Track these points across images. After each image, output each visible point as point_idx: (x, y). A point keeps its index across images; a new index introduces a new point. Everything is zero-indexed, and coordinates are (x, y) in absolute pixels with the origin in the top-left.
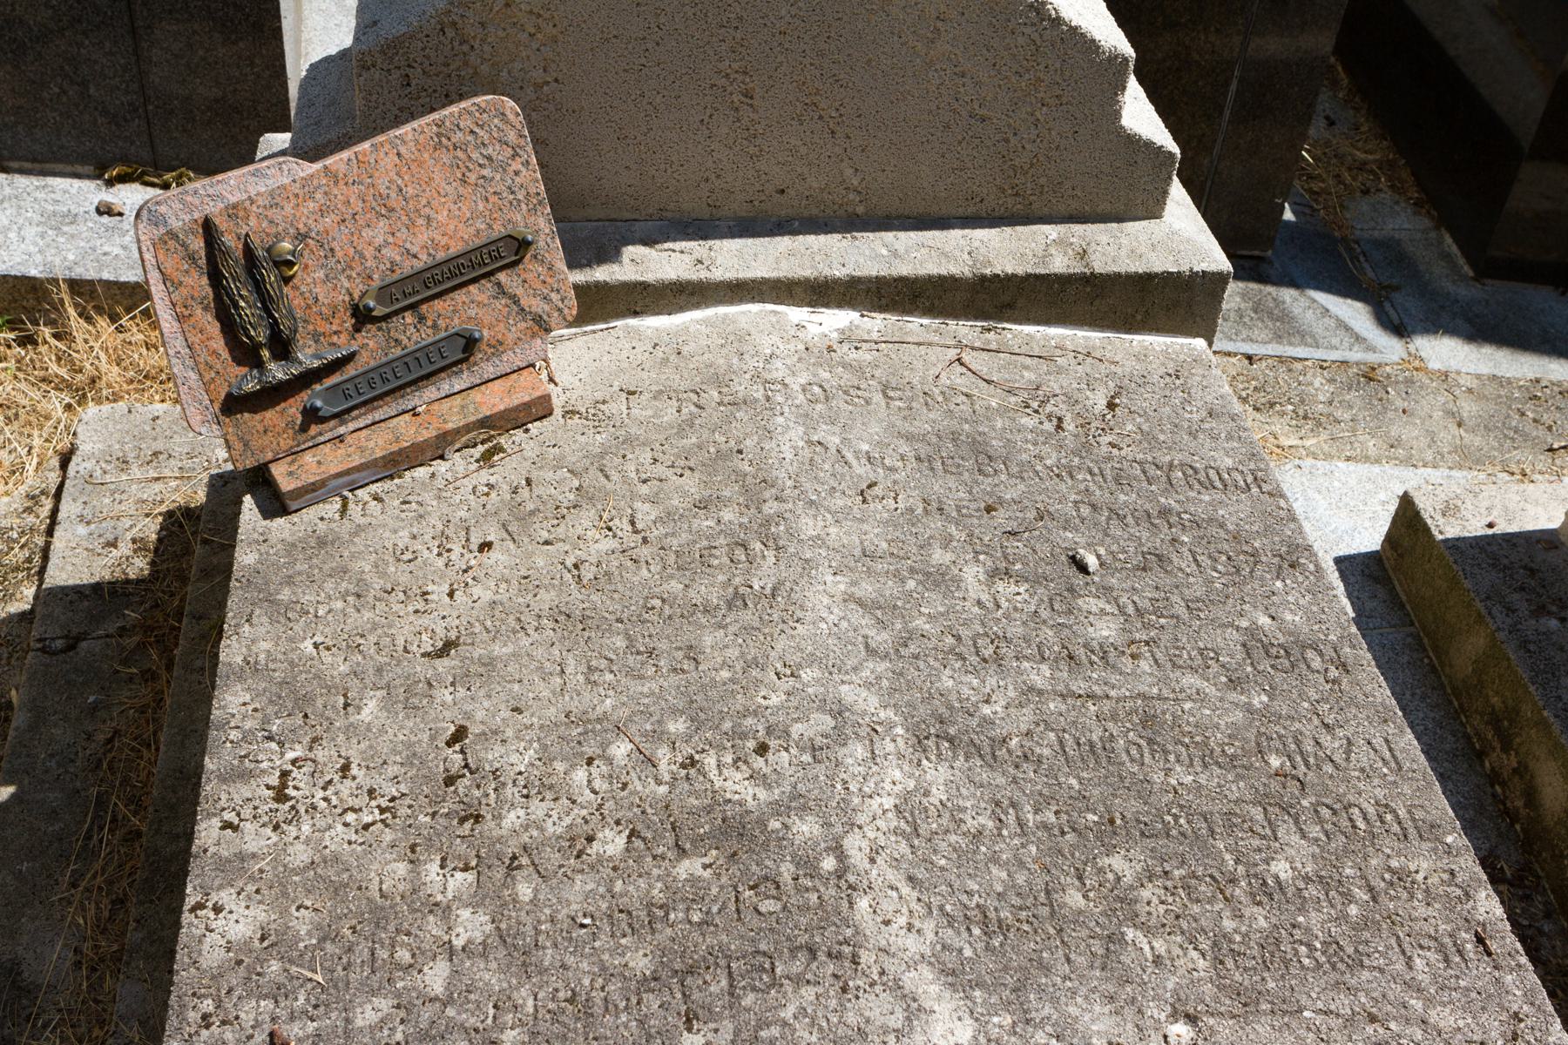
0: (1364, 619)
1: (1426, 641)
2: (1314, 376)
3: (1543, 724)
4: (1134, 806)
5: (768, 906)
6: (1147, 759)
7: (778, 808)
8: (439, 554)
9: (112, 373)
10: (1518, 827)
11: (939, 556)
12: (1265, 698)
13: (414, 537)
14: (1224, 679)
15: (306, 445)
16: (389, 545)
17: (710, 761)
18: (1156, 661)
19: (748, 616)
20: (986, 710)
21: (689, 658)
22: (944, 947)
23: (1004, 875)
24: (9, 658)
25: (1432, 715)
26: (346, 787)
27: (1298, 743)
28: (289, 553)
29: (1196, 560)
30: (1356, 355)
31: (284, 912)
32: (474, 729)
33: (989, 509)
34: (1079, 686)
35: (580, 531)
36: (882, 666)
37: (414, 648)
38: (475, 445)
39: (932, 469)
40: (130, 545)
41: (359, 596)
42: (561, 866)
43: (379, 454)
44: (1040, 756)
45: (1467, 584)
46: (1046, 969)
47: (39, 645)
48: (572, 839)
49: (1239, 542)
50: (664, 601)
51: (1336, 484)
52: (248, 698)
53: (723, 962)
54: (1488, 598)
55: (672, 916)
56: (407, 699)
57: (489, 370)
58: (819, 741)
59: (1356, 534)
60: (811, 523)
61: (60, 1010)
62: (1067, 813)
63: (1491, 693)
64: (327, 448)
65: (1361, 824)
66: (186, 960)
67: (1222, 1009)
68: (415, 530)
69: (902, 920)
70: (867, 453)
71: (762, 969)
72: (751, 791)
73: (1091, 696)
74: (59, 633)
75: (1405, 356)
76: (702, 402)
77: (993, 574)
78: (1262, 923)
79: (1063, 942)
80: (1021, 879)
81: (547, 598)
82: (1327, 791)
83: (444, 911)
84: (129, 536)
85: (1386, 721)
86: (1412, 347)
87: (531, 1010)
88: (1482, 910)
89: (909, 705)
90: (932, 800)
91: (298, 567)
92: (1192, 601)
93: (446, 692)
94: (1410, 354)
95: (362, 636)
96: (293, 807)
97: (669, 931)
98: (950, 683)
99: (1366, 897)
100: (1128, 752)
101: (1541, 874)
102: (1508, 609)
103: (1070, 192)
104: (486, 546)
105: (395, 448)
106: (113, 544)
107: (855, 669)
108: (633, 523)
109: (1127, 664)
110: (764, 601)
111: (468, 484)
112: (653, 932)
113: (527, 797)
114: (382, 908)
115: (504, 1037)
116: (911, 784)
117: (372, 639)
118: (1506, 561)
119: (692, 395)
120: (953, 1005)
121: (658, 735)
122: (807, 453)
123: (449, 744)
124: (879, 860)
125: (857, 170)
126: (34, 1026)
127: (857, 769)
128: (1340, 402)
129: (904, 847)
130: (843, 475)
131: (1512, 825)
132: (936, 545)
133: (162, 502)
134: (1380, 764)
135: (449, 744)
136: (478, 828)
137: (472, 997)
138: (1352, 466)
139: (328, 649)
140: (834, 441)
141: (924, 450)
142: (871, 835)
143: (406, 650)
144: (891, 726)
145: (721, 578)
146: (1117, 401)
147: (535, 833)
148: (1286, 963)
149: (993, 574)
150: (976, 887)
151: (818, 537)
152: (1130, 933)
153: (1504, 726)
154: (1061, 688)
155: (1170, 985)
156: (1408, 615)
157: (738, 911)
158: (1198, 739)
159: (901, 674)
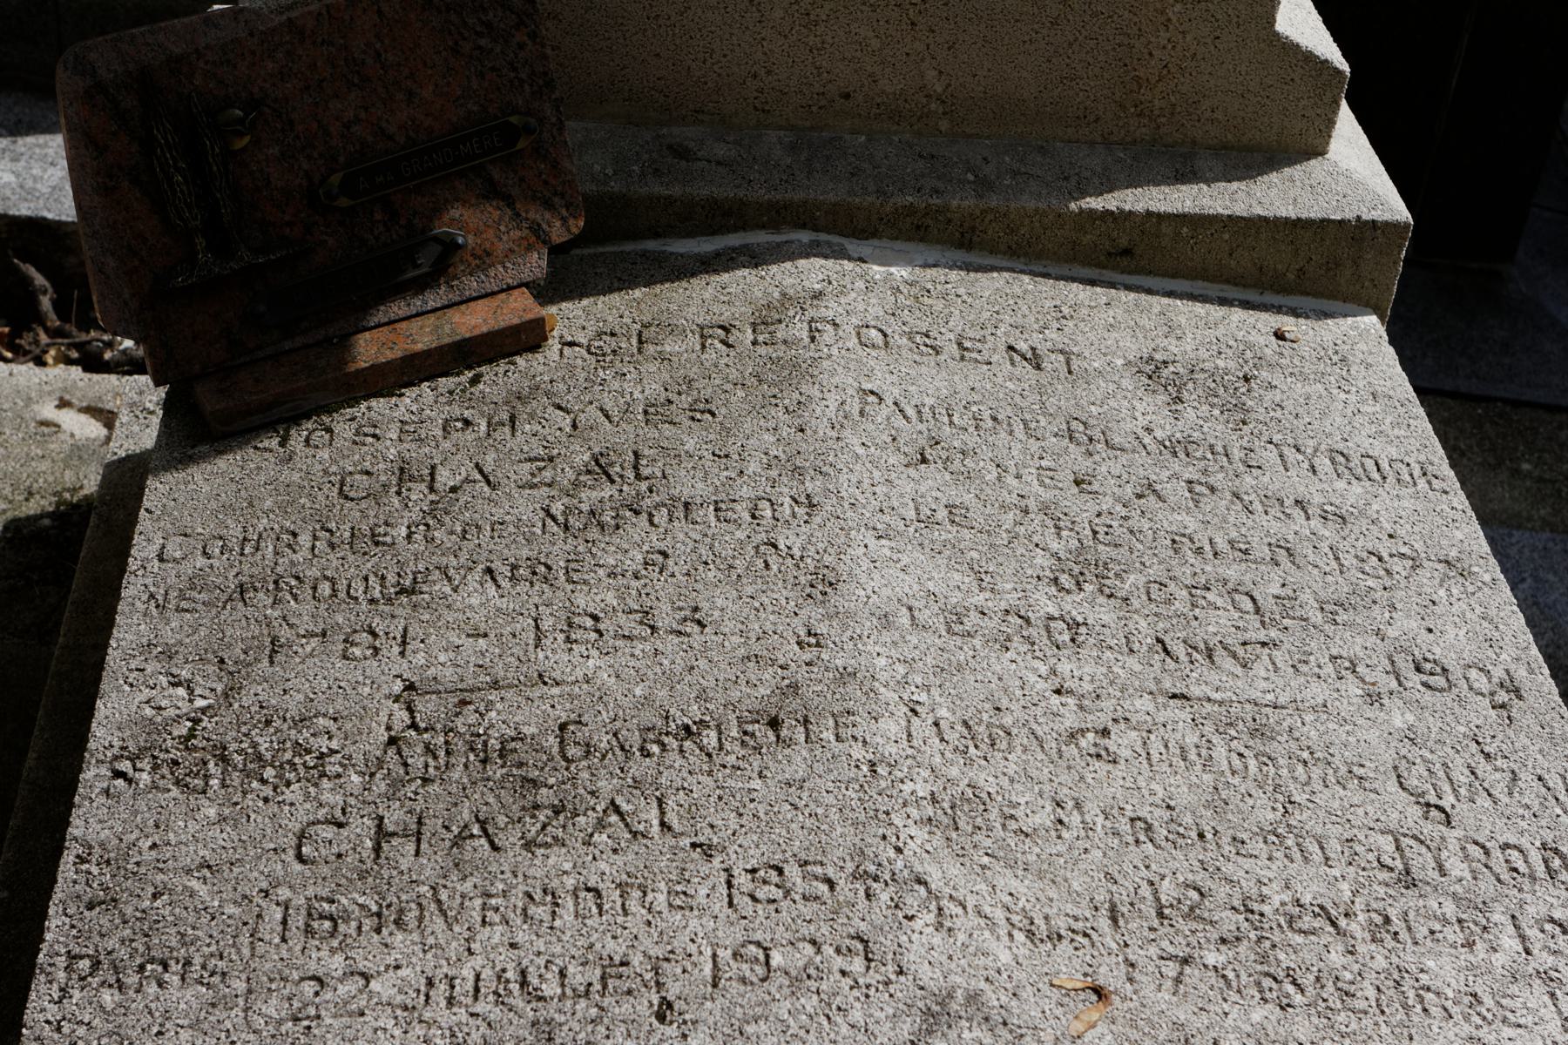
57: (472, 285)
76: (731, 340)
103: (1208, 114)
119: (720, 331)
125: (941, 72)
150: (1023, 890)
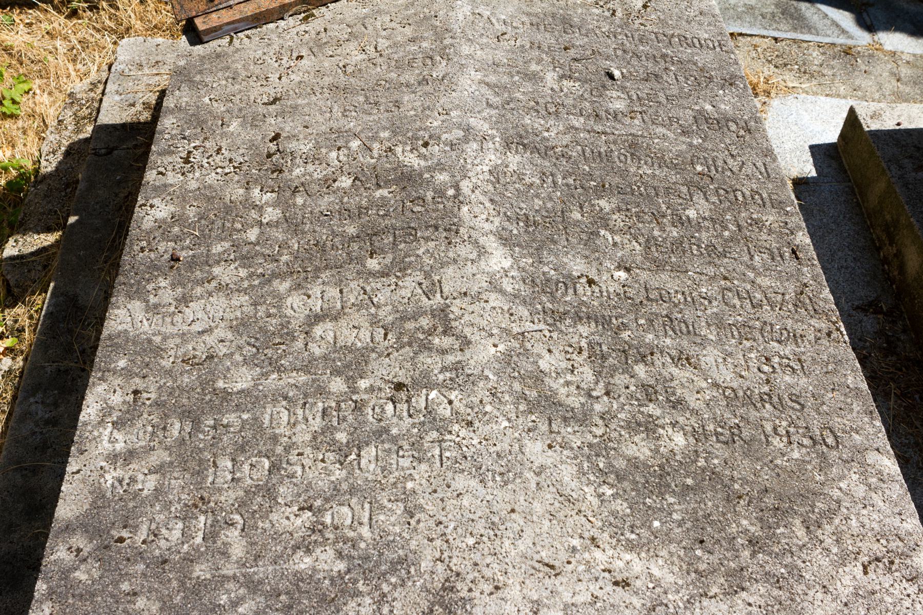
0: (822, 178)
1: (856, 190)
2: (814, 51)
3: (910, 226)
4: (617, 180)
5: (417, 209)
6: (629, 161)
7: (429, 169)
8: (276, 61)
9: (138, 25)
10: (894, 286)
11: (534, 67)
12: (700, 141)
13: (265, 54)
14: (679, 131)
15: (213, 9)
16: (252, 57)
17: (399, 150)
18: (643, 121)
19: (428, 88)
20: (546, 134)
21: (395, 106)
22: (503, 229)
23: (541, 203)
24: (78, 160)
25: (854, 228)
26: (218, 158)
27: (714, 161)
28: (201, 60)
29: (676, 78)
30: (841, 40)
31: (184, 208)
32: (284, 135)
33: (566, 49)
34: (599, 128)
35: (348, 51)
36: (493, 112)
37: (259, 101)
38: (300, 14)
39: (538, 29)
40: (142, 106)
41: (234, 79)
42: (319, 191)
43: (249, 14)
44: (571, 155)
45: (879, 154)
46: (555, 242)
47: (93, 152)
48: (326, 180)
49: (703, 72)
50: (386, 81)
51: (818, 108)
52: (175, 121)
53: (392, 231)
54: (889, 161)
55: (370, 212)
56: (252, 122)
58: (455, 142)
59: (824, 133)
60: (467, 48)
61: (96, 318)
62: (580, 180)
63: (886, 213)
64: (223, 11)
65: (740, 198)
66: (135, 226)
67: (645, 267)
68: (265, 51)
69: (484, 217)
70: (504, 20)
71: (410, 233)
72: (417, 162)
73: (604, 133)
74: (103, 146)
75: (871, 43)
77: (562, 77)
78: (675, 234)
79: (566, 232)
80: (549, 205)
81: (327, 80)
82: (725, 183)
83: (260, 209)
84: (141, 101)
85: (766, 156)
86: (876, 38)
87: (296, 249)
88: (798, 240)
89: (504, 129)
90: (509, 169)
91: (205, 66)
92: (670, 96)
93: (272, 120)
94: (874, 41)
95: (234, 96)
96: (192, 166)
97: (368, 218)
98: (529, 121)
99: (734, 229)
100: (619, 158)
101: (904, 310)
102: (900, 167)
104: (300, 57)
105: (258, 11)
106: (133, 105)
107: (479, 112)
108: (376, 48)
109: (627, 121)
110: (438, 82)
111: (295, 31)
112: (360, 218)
113: (306, 163)
114: (230, 207)
115: (282, 258)
116: (499, 162)
117: (238, 97)
118: (904, 143)
120: (503, 252)
121: (374, 138)
122: (471, 18)
123: (271, 141)
124: (476, 191)
126: (83, 324)
127: (472, 154)
128: (827, 65)
129: (490, 187)
130: (489, 29)
131: (891, 285)
132: (533, 63)
133: (159, 85)
134: (758, 174)
135: (271, 141)
136: (280, 175)
137: (269, 242)
138: (828, 99)
139: (216, 101)
140: (487, 13)
141: (535, 20)
142: (474, 180)
143: (255, 102)
144: (493, 137)
145: (417, 72)
146: (649, 4)
147: (308, 177)
148: (684, 252)
149: (562, 77)
151: (470, 55)
152: (602, 232)
153: (891, 230)
154: (589, 128)
155: (619, 255)
156: (848, 176)
157: (403, 211)
158: (658, 155)
159: (503, 116)
